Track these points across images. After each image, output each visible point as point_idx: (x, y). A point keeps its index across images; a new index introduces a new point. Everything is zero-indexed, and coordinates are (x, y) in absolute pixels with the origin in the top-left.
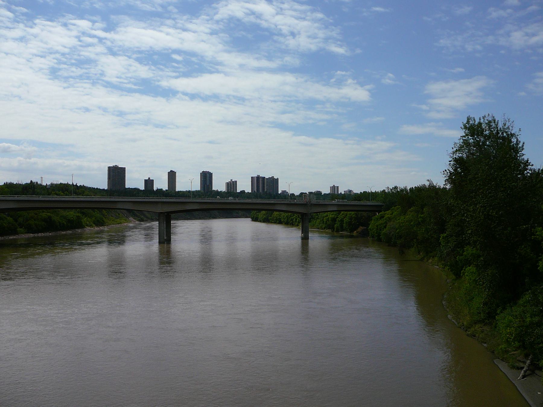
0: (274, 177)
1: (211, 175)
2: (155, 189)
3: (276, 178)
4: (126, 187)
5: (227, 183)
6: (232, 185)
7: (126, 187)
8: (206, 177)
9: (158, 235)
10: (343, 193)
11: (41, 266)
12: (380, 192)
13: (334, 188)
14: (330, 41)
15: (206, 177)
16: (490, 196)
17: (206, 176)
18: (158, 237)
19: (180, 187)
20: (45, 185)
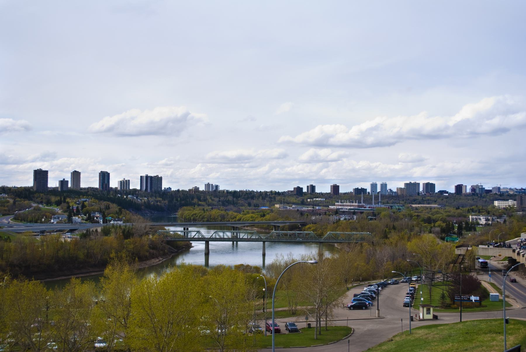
0: (158, 175)
1: (108, 174)
2: (163, 189)
3: (160, 176)
4: (81, 187)
5: (120, 181)
6: (125, 183)
7: (81, 187)
8: (104, 177)
9: (210, 249)
10: (395, 190)
11: (13, 345)
12: (248, 191)
13: (358, 188)
14: (400, 163)
15: (104, 177)
16: (168, 285)
17: (104, 176)
18: (265, 245)
19: (83, 185)
20: (361, 188)
